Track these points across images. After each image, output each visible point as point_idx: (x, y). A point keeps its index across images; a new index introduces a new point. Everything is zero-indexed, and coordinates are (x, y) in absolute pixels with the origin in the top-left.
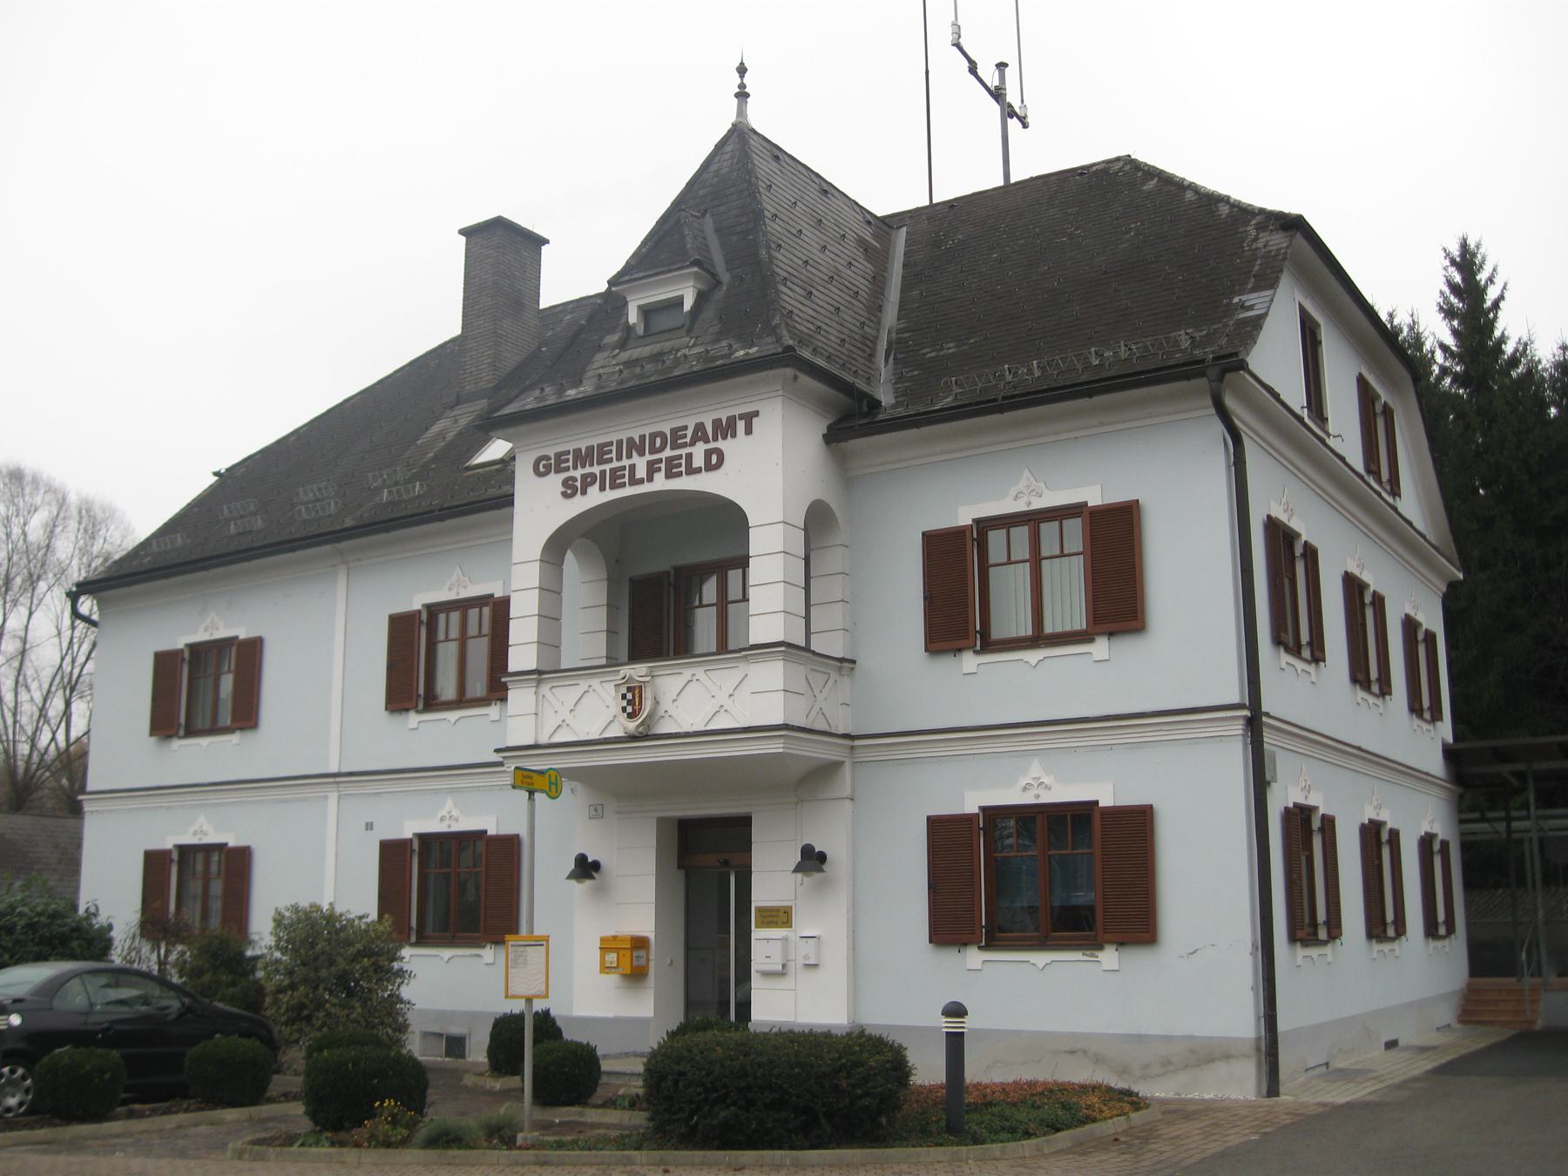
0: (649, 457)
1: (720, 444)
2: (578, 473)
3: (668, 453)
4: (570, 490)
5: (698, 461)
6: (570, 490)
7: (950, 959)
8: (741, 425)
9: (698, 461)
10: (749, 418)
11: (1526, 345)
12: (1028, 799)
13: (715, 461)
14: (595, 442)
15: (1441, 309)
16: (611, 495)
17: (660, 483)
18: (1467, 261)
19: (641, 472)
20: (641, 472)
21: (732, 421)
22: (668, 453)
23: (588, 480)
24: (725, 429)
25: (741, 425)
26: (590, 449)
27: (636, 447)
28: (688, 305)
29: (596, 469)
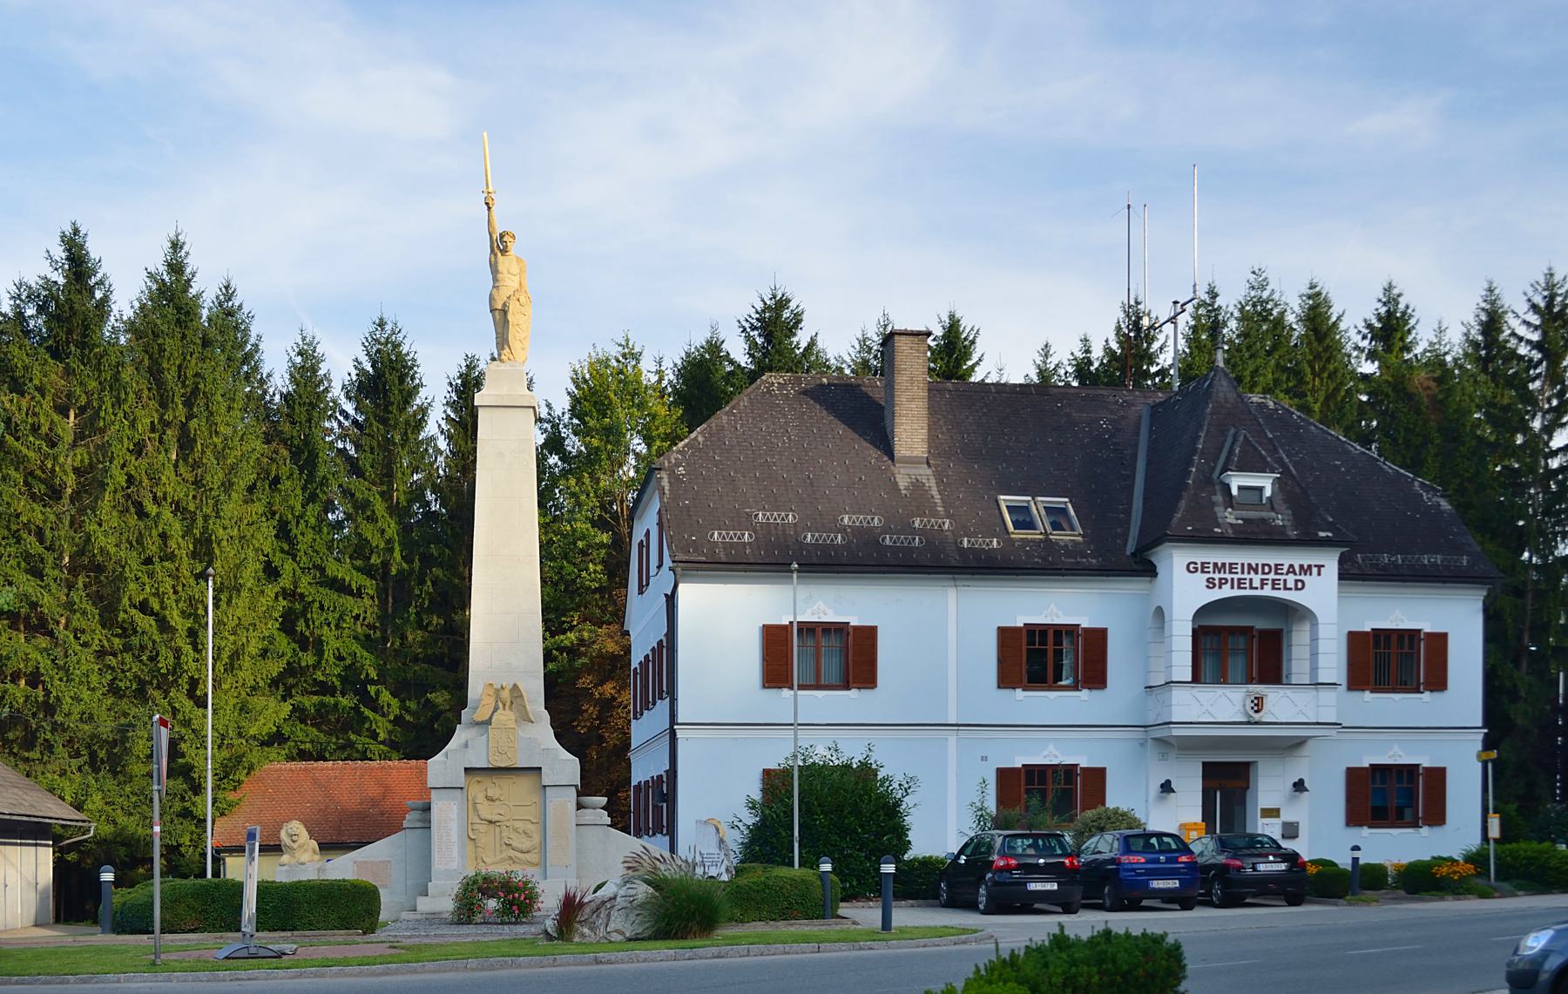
0: (1260, 576)
1: (1302, 577)
2: (1217, 576)
3: (1272, 576)
4: (1211, 584)
5: (1291, 584)
6: (1211, 584)
7: (1354, 831)
8: (1315, 570)
9: (1291, 584)
10: (1319, 567)
11: (227, 288)
12: (815, 619)
13: (1300, 586)
14: (1227, 562)
15: (63, 236)
16: (1237, 593)
17: (1267, 591)
18: (176, 246)
19: (1256, 583)
20: (1256, 583)
21: (1310, 567)
22: (1272, 576)
23: (1222, 582)
24: (1306, 570)
25: (1315, 570)
26: (1224, 565)
27: (1253, 569)
28: (1268, 493)
29: (1228, 576)
